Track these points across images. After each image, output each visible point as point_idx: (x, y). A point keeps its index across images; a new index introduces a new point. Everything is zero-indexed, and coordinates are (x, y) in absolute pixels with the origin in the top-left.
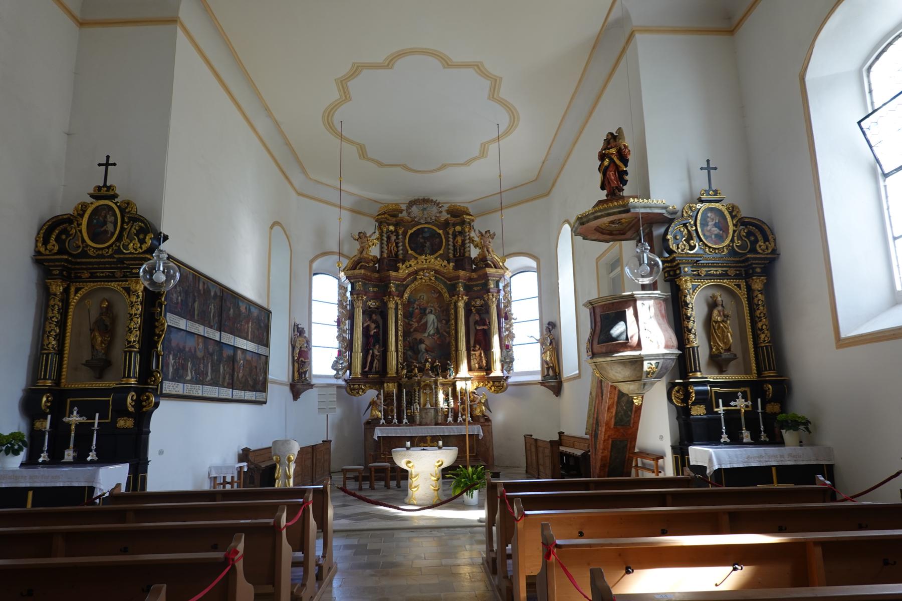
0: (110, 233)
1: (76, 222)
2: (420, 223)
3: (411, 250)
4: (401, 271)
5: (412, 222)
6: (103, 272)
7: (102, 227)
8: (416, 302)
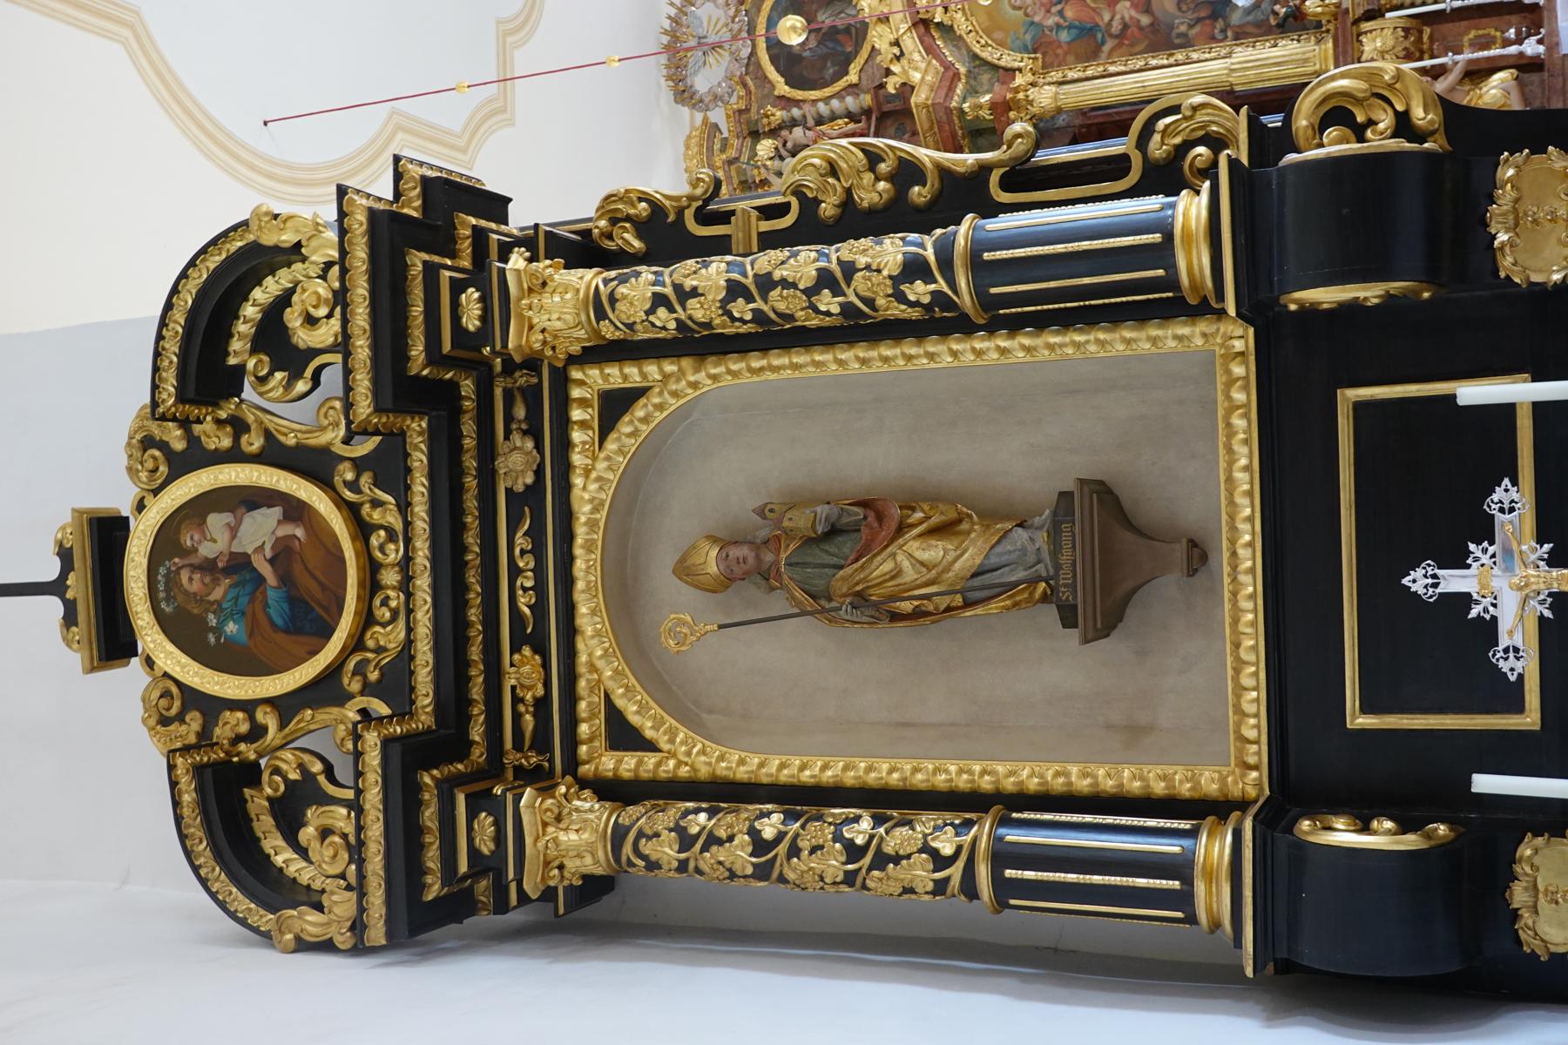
0: (287, 530)
1: (242, 747)
2: (749, 58)
3: (846, 73)
4: (916, 77)
5: (745, 85)
6: (515, 572)
7: (260, 580)
8: (1037, 19)
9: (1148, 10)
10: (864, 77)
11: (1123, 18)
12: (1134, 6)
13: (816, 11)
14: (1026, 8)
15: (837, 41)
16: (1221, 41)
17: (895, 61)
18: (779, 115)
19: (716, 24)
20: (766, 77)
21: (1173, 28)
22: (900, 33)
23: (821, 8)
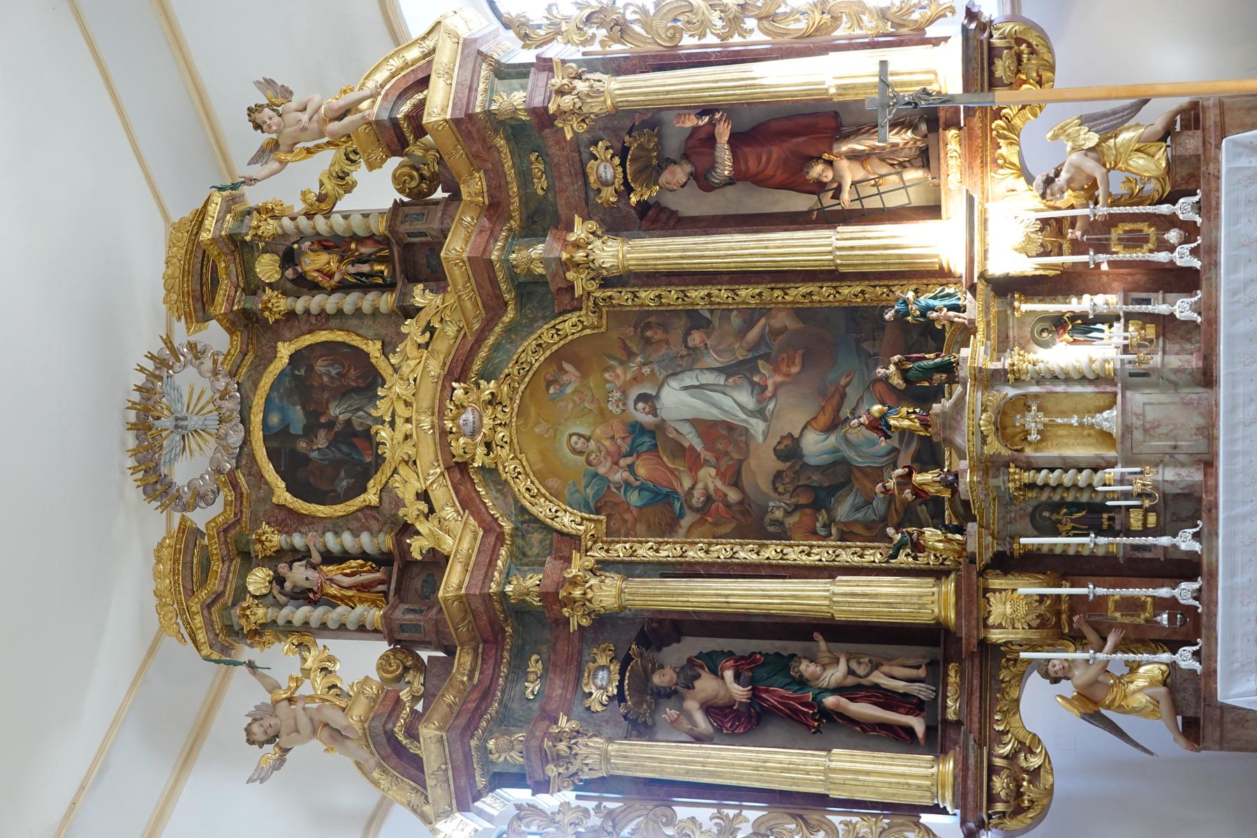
2: (241, 447)
3: (364, 490)
4: (448, 544)
5: (235, 485)
8: (602, 470)
9: (736, 484)
10: (386, 498)
11: (706, 488)
12: (721, 475)
13: (328, 401)
14: (589, 455)
15: (353, 446)
16: (824, 538)
17: (422, 518)
18: (276, 540)
19: (198, 400)
20: (262, 476)
21: (766, 512)
22: (429, 482)
23: (335, 399)
